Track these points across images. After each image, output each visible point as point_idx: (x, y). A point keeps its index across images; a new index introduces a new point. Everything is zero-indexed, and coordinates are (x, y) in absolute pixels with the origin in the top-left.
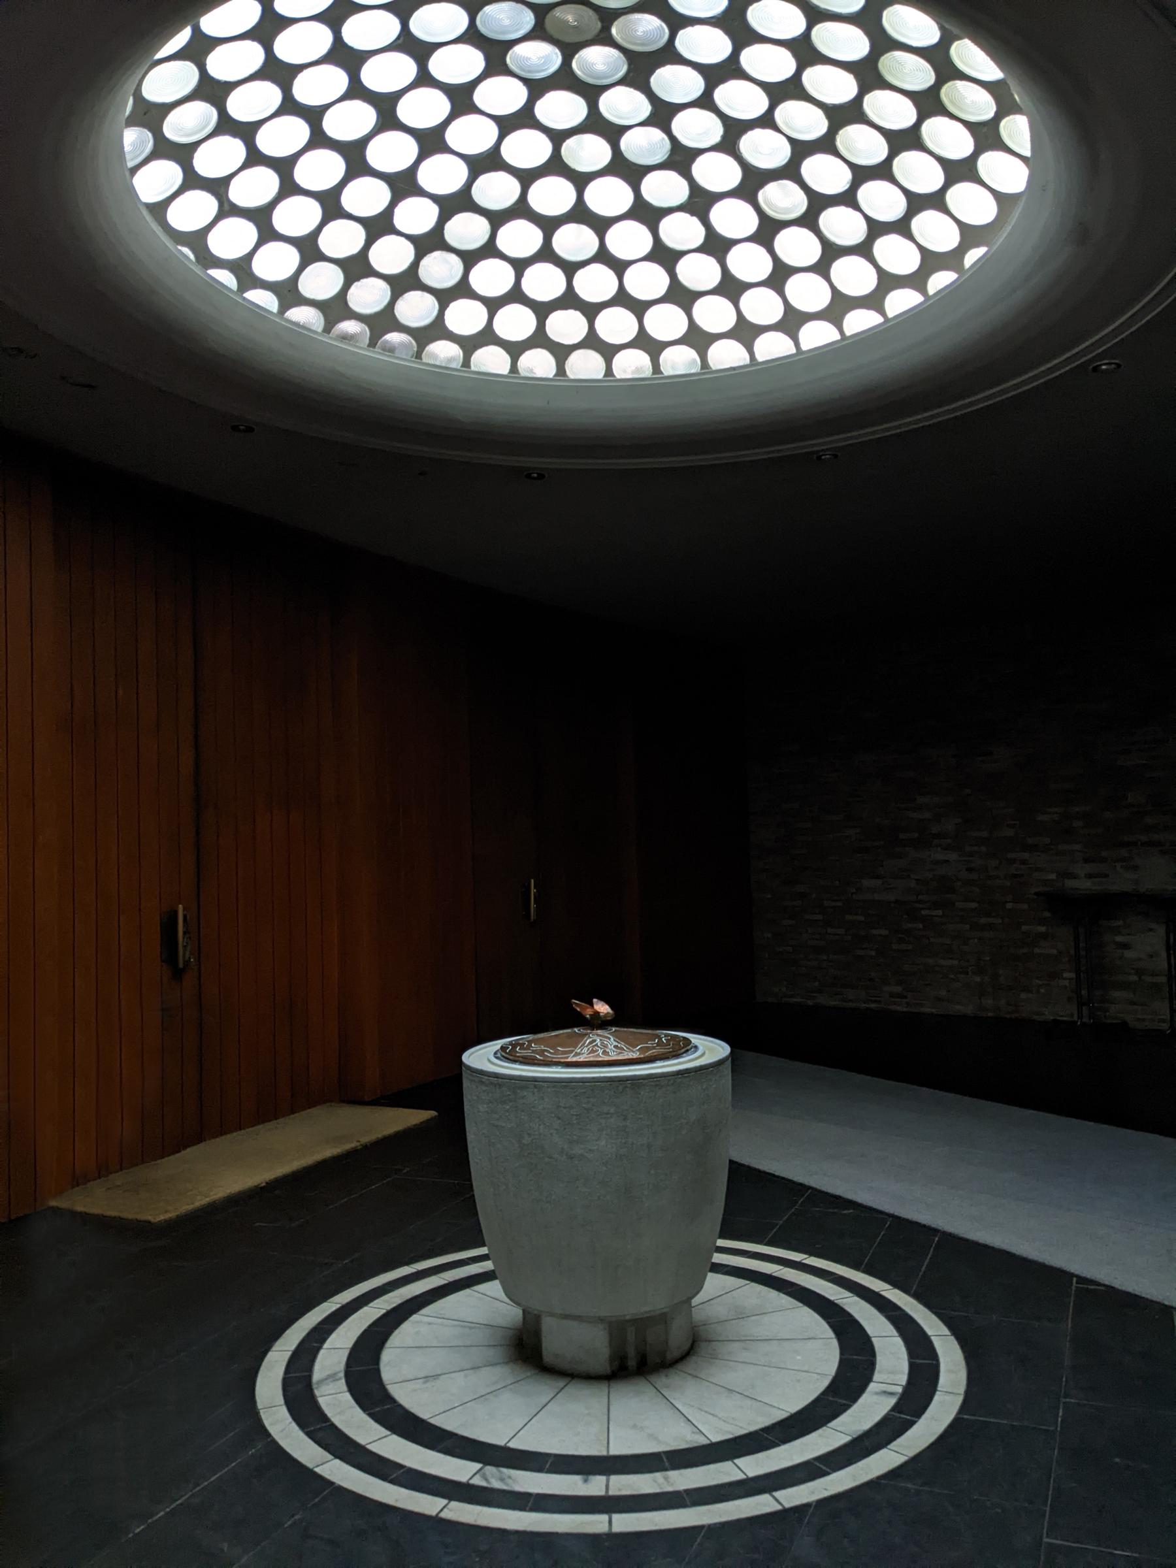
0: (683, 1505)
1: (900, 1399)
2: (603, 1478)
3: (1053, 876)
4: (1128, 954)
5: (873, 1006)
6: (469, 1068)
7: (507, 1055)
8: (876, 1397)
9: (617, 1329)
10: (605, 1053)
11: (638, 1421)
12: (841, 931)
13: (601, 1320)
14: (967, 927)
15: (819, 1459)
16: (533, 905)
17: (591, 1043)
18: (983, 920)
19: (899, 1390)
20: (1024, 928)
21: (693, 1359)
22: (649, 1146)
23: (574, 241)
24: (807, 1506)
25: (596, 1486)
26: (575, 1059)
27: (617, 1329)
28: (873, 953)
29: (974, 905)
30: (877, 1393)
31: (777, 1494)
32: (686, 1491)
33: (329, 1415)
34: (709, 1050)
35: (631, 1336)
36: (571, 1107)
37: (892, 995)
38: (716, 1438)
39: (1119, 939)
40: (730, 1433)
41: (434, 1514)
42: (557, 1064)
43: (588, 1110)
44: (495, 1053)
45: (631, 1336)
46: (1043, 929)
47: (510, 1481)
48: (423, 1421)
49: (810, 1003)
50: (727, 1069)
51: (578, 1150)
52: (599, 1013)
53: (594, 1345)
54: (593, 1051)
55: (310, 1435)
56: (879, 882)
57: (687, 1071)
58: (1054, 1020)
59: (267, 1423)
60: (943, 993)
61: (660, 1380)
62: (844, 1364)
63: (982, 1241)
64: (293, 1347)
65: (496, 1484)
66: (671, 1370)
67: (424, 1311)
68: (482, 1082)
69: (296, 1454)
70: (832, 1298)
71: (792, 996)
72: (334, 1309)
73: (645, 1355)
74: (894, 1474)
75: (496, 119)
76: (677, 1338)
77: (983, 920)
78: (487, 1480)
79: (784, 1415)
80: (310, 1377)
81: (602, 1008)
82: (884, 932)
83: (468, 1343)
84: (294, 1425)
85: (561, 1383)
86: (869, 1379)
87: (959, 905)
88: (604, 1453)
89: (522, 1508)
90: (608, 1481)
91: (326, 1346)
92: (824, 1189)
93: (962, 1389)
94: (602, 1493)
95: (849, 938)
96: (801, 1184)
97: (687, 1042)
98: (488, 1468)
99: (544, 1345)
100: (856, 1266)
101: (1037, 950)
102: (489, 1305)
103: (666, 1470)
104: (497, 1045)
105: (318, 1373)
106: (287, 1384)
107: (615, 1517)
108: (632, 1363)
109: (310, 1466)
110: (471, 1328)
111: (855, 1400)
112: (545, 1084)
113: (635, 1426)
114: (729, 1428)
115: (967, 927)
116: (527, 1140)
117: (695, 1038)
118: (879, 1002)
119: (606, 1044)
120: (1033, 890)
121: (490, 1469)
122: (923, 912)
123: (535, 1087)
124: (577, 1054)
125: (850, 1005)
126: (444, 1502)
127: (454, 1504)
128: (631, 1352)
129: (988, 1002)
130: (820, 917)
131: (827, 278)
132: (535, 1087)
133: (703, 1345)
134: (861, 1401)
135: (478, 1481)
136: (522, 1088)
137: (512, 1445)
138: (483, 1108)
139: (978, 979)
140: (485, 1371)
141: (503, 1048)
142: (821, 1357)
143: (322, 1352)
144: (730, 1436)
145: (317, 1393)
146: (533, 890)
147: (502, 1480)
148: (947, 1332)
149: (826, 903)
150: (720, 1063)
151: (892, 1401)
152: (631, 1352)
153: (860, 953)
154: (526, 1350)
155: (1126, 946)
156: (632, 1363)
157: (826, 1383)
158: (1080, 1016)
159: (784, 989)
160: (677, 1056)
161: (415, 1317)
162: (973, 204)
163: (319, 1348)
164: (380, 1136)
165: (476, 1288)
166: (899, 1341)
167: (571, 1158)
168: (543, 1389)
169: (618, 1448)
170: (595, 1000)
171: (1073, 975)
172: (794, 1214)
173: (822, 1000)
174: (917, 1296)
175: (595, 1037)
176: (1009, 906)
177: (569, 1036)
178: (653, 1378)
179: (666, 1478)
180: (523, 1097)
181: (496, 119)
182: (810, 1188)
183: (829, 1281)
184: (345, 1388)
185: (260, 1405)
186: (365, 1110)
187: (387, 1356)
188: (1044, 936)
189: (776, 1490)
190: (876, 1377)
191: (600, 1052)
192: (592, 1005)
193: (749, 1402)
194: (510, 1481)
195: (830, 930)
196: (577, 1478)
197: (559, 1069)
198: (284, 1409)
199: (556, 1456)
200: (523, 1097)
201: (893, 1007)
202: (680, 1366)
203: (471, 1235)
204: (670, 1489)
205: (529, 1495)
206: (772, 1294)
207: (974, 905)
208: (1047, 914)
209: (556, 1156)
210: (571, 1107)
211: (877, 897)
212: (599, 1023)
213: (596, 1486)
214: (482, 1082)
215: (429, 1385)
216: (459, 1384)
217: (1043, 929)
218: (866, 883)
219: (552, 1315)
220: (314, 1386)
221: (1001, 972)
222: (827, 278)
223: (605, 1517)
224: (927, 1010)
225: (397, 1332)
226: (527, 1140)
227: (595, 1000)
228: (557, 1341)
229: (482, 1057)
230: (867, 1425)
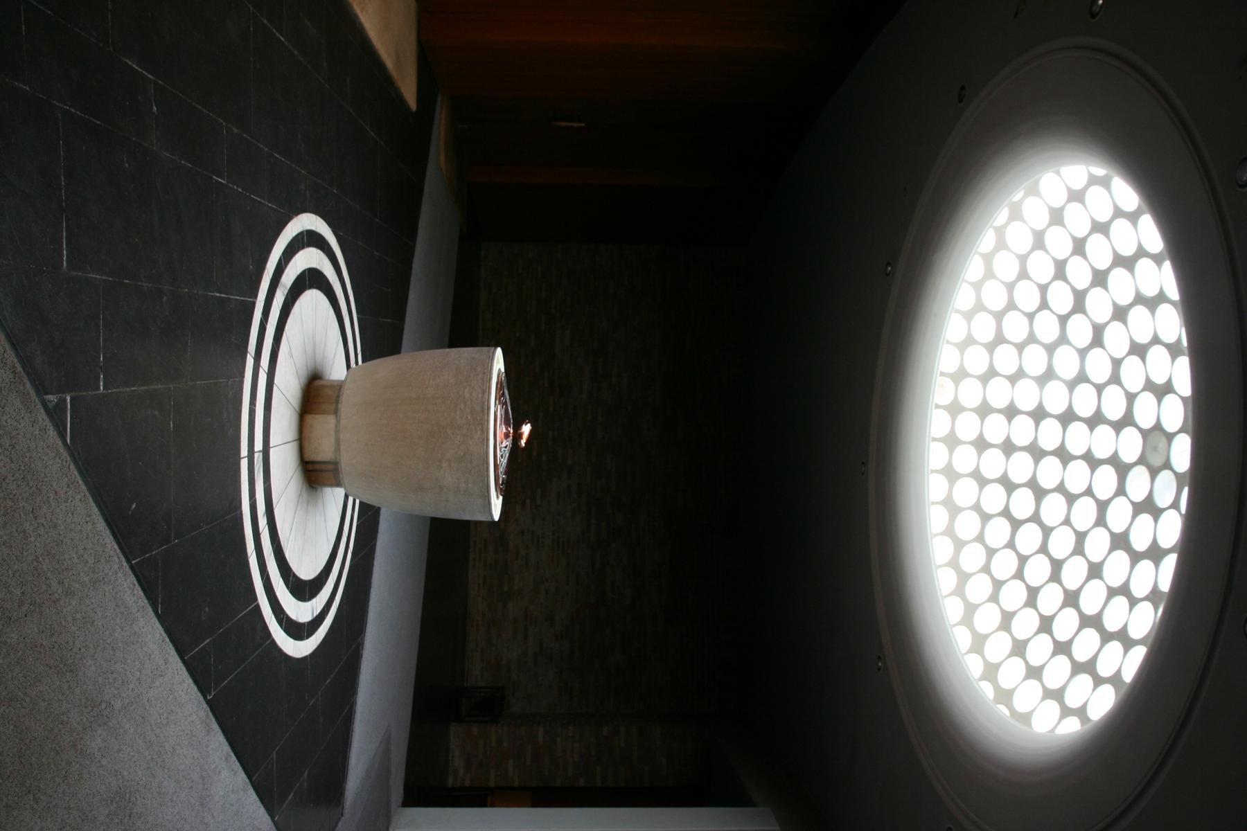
3: (570, 462)
4: (518, 507)
11: (284, 462)
16: (564, 124)
23: (1035, 360)
25: (259, 446)
29: (551, 409)
39: (528, 502)
73: (314, 474)
75: (1014, 613)
99: (317, 416)
102: (337, 371)
111: (291, 592)
131: (999, 515)
146: (576, 125)
154: (315, 395)
155: (524, 505)
156: (310, 467)
162: (1027, 697)
169: (272, 451)
176: (551, 433)
181: (1014, 613)
203: (379, 509)
207: (551, 409)
222: (999, 515)
228: (323, 425)
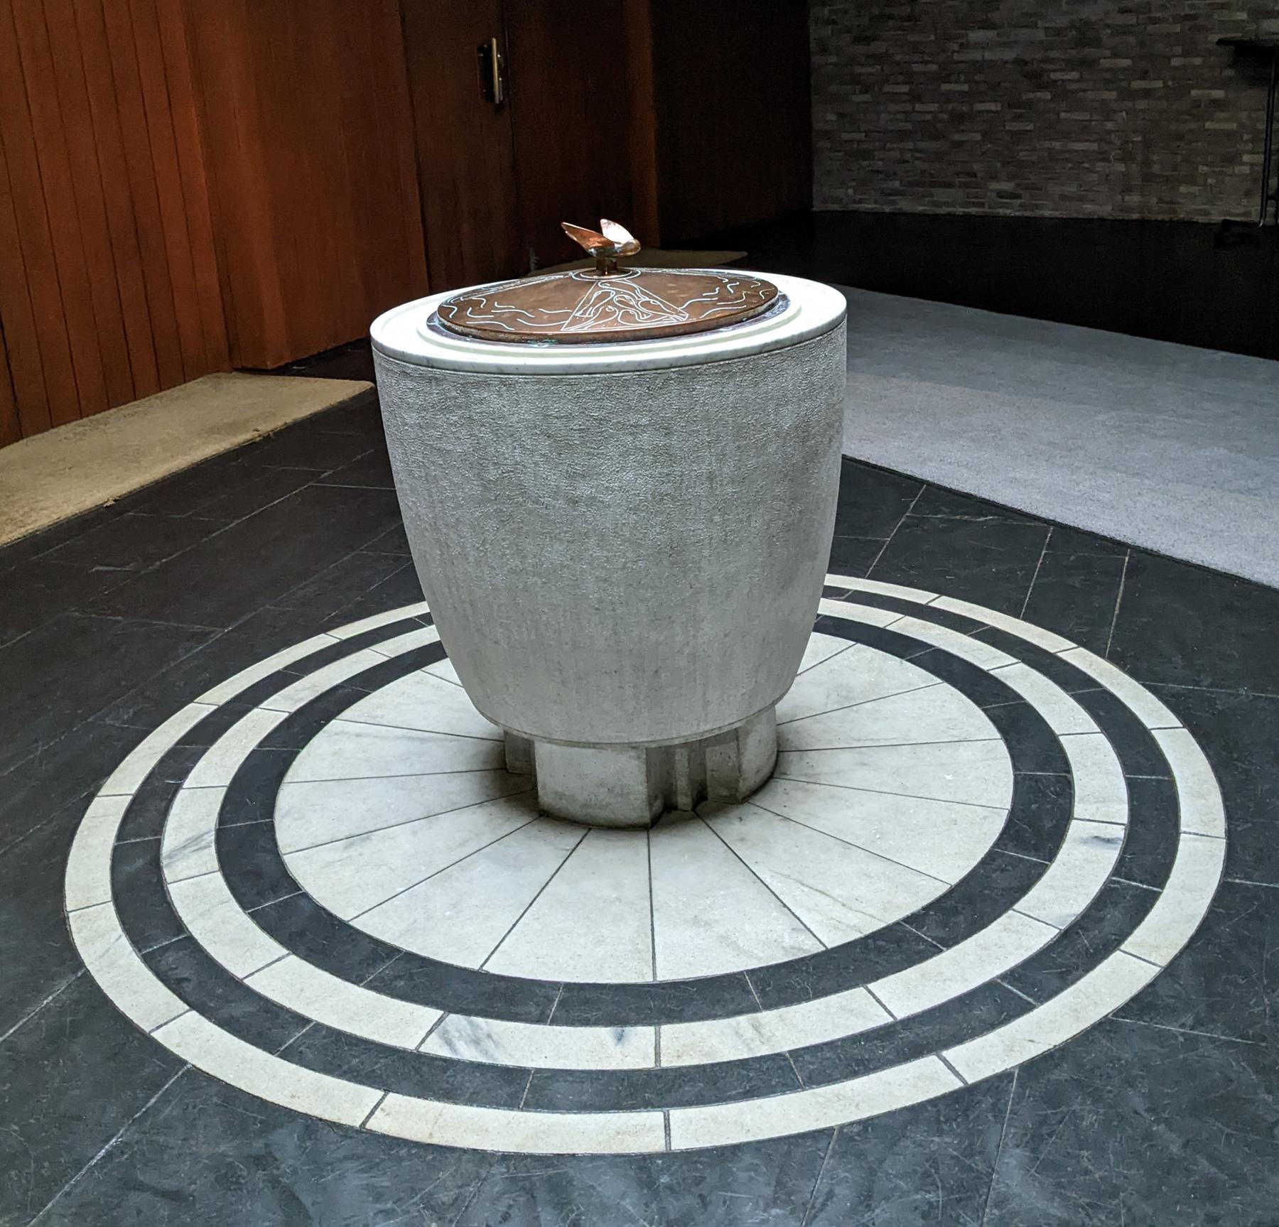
0: (789, 1085)
1: (1124, 851)
2: (649, 1031)
3: (1243, 16)
5: (973, 210)
6: (383, 349)
7: (448, 323)
8: (1084, 848)
9: (659, 760)
10: (626, 316)
12: (934, 107)
13: (634, 747)
14: (1114, 95)
15: (1012, 975)
17: (600, 298)
18: (1137, 84)
19: (1120, 832)
20: (1194, 92)
21: (780, 786)
22: (711, 478)
24: (1004, 1077)
25: (634, 1049)
26: (573, 330)
27: (659, 760)
28: (978, 137)
29: (1126, 62)
30: (1085, 842)
31: (951, 1054)
32: (795, 1053)
33: (185, 919)
34: (811, 303)
35: (681, 762)
36: (570, 417)
37: (1001, 194)
38: (834, 940)
40: (854, 927)
41: (357, 1124)
42: (541, 339)
43: (600, 421)
44: (430, 319)
45: (681, 762)
46: (1218, 94)
47: (490, 1045)
48: (343, 925)
49: (887, 209)
50: (841, 337)
51: (584, 489)
52: (612, 244)
53: (623, 780)
54: (605, 315)
55: (148, 960)
56: (992, 34)
57: (778, 346)
58: (1225, 221)
59: (78, 939)
60: (1072, 189)
61: (735, 828)
62: (1024, 789)
63: (1197, 560)
64: (134, 789)
65: (467, 1053)
66: (747, 809)
67: (347, 714)
68: (405, 374)
69: (123, 1003)
70: (985, 668)
71: (860, 201)
72: (205, 714)
74: (1142, 1004)
76: (754, 757)
77: (1137, 84)
78: (449, 1043)
79: (942, 889)
80: (158, 843)
81: (616, 234)
82: (992, 106)
83: (418, 769)
84: (125, 941)
85: (569, 839)
86: (1066, 816)
87: (1105, 63)
88: (649, 979)
89: (511, 1103)
90: (658, 1035)
91: (187, 784)
92: (946, 483)
93: (1220, 827)
94: (649, 1064)
95: (945, 116)
96: (910, 478)
97: (771, 290)
98: (453, 1018)
100: (1013, 611)
101: (1208, 125)
103: (755, 1009)
104: (430, 304)
105: (171, 839)
106: (119, 856)
107: (677, 1114)
108: (684, 800)
109: (146, 1026)
110: (423, 740)
112: (521, 379)
113: (695, 921)
114: (853, 918)
115: (1114, 95)
116: (492, 474)
117: (783, 282)
118: (982, 205)
119: (626, 298)
120: (1216, 38)
121: (456, 1021)
122: (1053, 76)
123: (502, 382)
124: (576, 321)
125: (944, 210)
126: (375, 1094)
127: (395, 1100)
128: (682, 783)
129: (1134, 199)
130: (905, 89)
132: (502, 382)
133: (793, 756)
134: (1062, 855)
135: (434, 1047)
136: (478, 385)
137: (492, 968)
138: (412, 418)
139: (1121, 167)
140: (447, 821)
141: (443, 311)
142: (986, 781)
143: (181, 795)
144: (857, 936)
145: (168, 874)
146: (496, 56)
147: (476, 1042)
148: (1176, 722)
149: (916, 68)
150: (832, 326)
151: (1111, 856)
152: (682, 783)
153: (957, 137)
154: (511, 779)
156: (684, 800)
157: (998, 824)
158: (1263, 214)
159: (851, 191)
160: (756, 317)
161: (334, 725)
163: (178, 788)
164: (289, 420)
165: (429, 668)
166: (1102, 740)
167: (574, 502)
168: (545, 848)
170: (603, 221)
171: (1260, 158)
172: (904, 526)
173: (906, 205)
174: (1117, 659)
175: (607, 288)
176: (1175, 62)
177: (561, 286)
178: (720, 825)
179: (756, 1028)
180: (481, 402)
182: (922, 482)
183: (976, 637)
184: (215, 864)
185: (70, 904)
186: (269, 382)
187: (288, 797)
188: (1217, 104)
189: (947, 1046)
190: (1078, 810)
191: (619, 314)
192: (599, 229)
193: (877, 867)
194: (490, 1045)
195: (918, 107)
196: (604, 1033)
197: (544, 349)
198: (111, 907)
199: (569, 987)
200: (481, 402)
201: (1001, 211)
202: (758, 799)
204: (765, 1051)
205: (521, 1072)
206: (892, 663)
207: (1126, 62)
208: (1230, 72)
209: (547, 500)
210: (570, 417)
211: (988, 55)
212: (609, 262)
213: (634, 1049)
214: (405, 374)
215: (353, 852)
216: (404, 849)
217: (1218, 94)
218: (976, 36)
219: (551, 741)
220: (164, 862)
221: (1155, 158)
223: (656, 1117)
224: (1047, 213)
225: (304, 753)
226: (492, 474)
227: (603, 221)
228: (558, 774)
229: (404, 329)
230: (1077, 904)
